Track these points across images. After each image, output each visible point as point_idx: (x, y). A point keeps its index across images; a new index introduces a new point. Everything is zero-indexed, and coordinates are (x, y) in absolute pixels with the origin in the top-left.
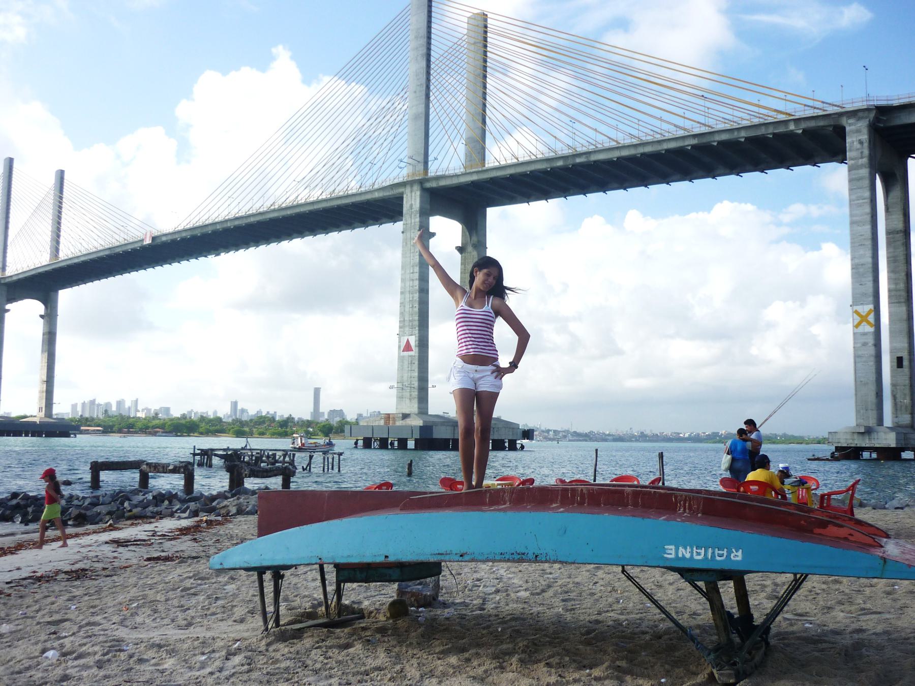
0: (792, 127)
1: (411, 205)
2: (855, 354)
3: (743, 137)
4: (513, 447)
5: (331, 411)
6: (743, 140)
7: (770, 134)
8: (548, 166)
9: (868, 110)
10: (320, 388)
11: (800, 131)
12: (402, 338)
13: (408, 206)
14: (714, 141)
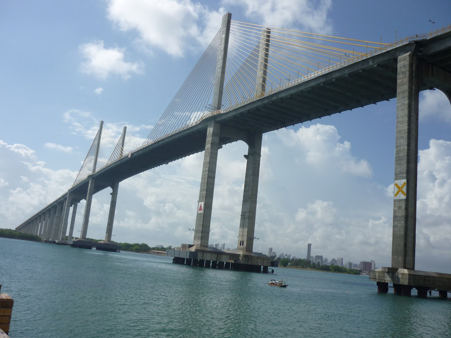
0: (371, 63)
1: (210, 131)
2: (394, 215)
3: (347, 74)
4: (265, 271)
5: (316, 256)
6: (347, 76)
7: (360, 70)
8: (262, 103)
9: (409, 44)
10: (311, 244)
11: (376, 66)
12: (199, 203)
13: (209, 131)
14: (333, 79)
